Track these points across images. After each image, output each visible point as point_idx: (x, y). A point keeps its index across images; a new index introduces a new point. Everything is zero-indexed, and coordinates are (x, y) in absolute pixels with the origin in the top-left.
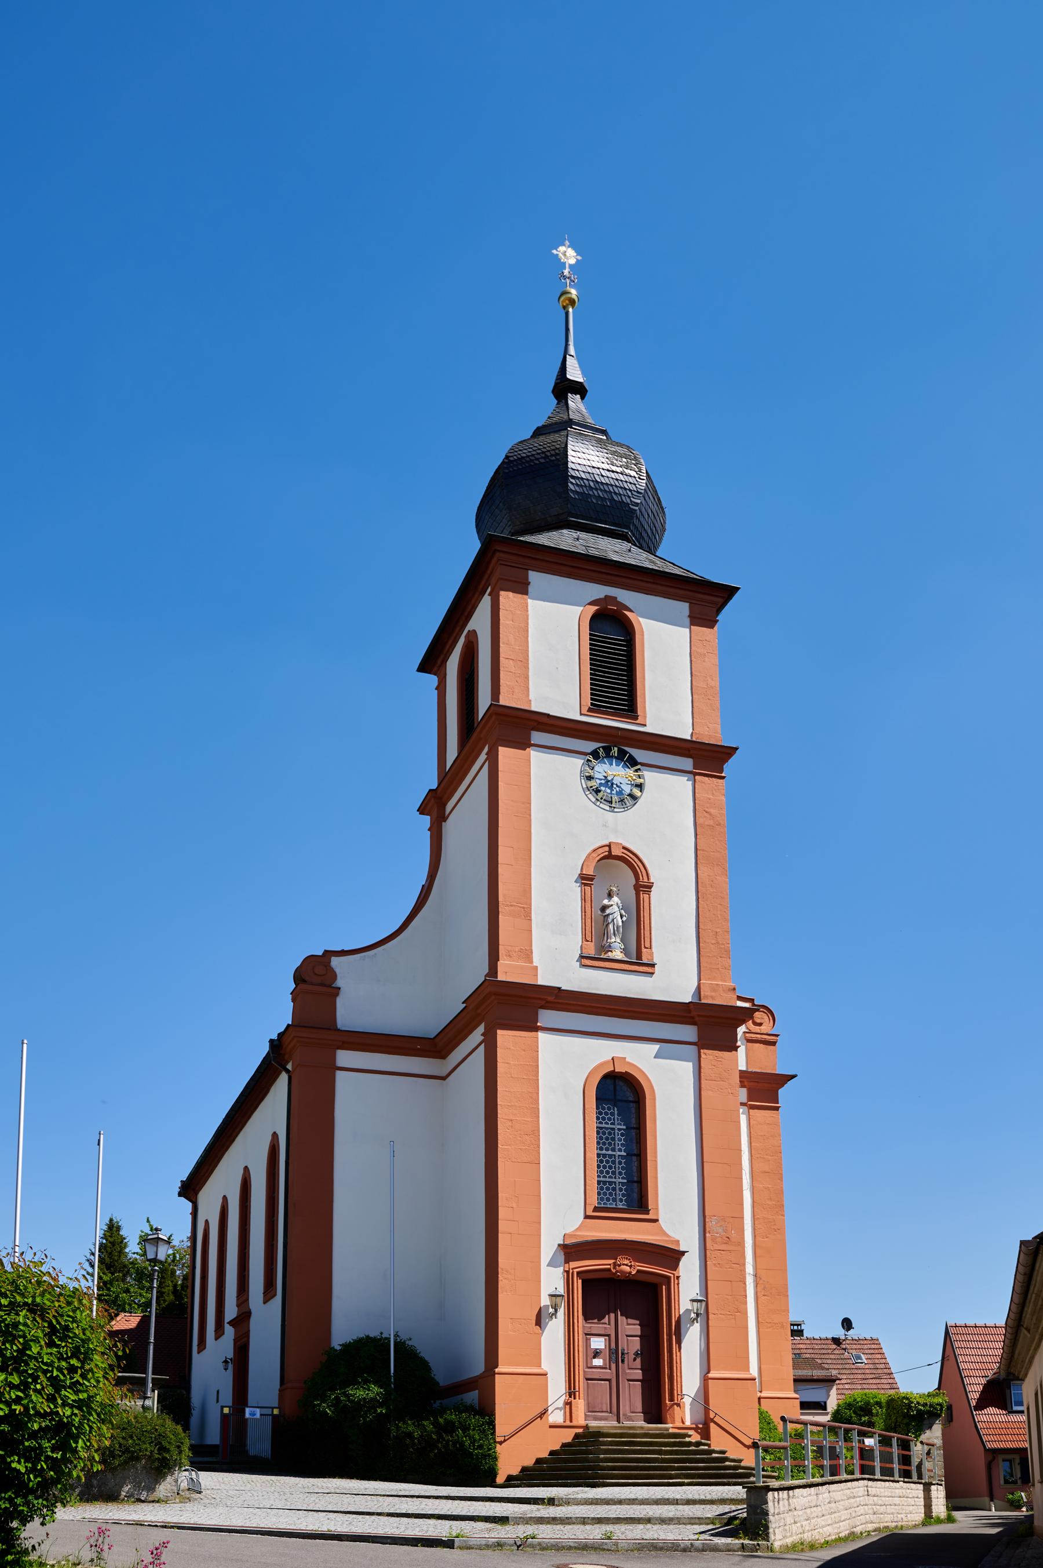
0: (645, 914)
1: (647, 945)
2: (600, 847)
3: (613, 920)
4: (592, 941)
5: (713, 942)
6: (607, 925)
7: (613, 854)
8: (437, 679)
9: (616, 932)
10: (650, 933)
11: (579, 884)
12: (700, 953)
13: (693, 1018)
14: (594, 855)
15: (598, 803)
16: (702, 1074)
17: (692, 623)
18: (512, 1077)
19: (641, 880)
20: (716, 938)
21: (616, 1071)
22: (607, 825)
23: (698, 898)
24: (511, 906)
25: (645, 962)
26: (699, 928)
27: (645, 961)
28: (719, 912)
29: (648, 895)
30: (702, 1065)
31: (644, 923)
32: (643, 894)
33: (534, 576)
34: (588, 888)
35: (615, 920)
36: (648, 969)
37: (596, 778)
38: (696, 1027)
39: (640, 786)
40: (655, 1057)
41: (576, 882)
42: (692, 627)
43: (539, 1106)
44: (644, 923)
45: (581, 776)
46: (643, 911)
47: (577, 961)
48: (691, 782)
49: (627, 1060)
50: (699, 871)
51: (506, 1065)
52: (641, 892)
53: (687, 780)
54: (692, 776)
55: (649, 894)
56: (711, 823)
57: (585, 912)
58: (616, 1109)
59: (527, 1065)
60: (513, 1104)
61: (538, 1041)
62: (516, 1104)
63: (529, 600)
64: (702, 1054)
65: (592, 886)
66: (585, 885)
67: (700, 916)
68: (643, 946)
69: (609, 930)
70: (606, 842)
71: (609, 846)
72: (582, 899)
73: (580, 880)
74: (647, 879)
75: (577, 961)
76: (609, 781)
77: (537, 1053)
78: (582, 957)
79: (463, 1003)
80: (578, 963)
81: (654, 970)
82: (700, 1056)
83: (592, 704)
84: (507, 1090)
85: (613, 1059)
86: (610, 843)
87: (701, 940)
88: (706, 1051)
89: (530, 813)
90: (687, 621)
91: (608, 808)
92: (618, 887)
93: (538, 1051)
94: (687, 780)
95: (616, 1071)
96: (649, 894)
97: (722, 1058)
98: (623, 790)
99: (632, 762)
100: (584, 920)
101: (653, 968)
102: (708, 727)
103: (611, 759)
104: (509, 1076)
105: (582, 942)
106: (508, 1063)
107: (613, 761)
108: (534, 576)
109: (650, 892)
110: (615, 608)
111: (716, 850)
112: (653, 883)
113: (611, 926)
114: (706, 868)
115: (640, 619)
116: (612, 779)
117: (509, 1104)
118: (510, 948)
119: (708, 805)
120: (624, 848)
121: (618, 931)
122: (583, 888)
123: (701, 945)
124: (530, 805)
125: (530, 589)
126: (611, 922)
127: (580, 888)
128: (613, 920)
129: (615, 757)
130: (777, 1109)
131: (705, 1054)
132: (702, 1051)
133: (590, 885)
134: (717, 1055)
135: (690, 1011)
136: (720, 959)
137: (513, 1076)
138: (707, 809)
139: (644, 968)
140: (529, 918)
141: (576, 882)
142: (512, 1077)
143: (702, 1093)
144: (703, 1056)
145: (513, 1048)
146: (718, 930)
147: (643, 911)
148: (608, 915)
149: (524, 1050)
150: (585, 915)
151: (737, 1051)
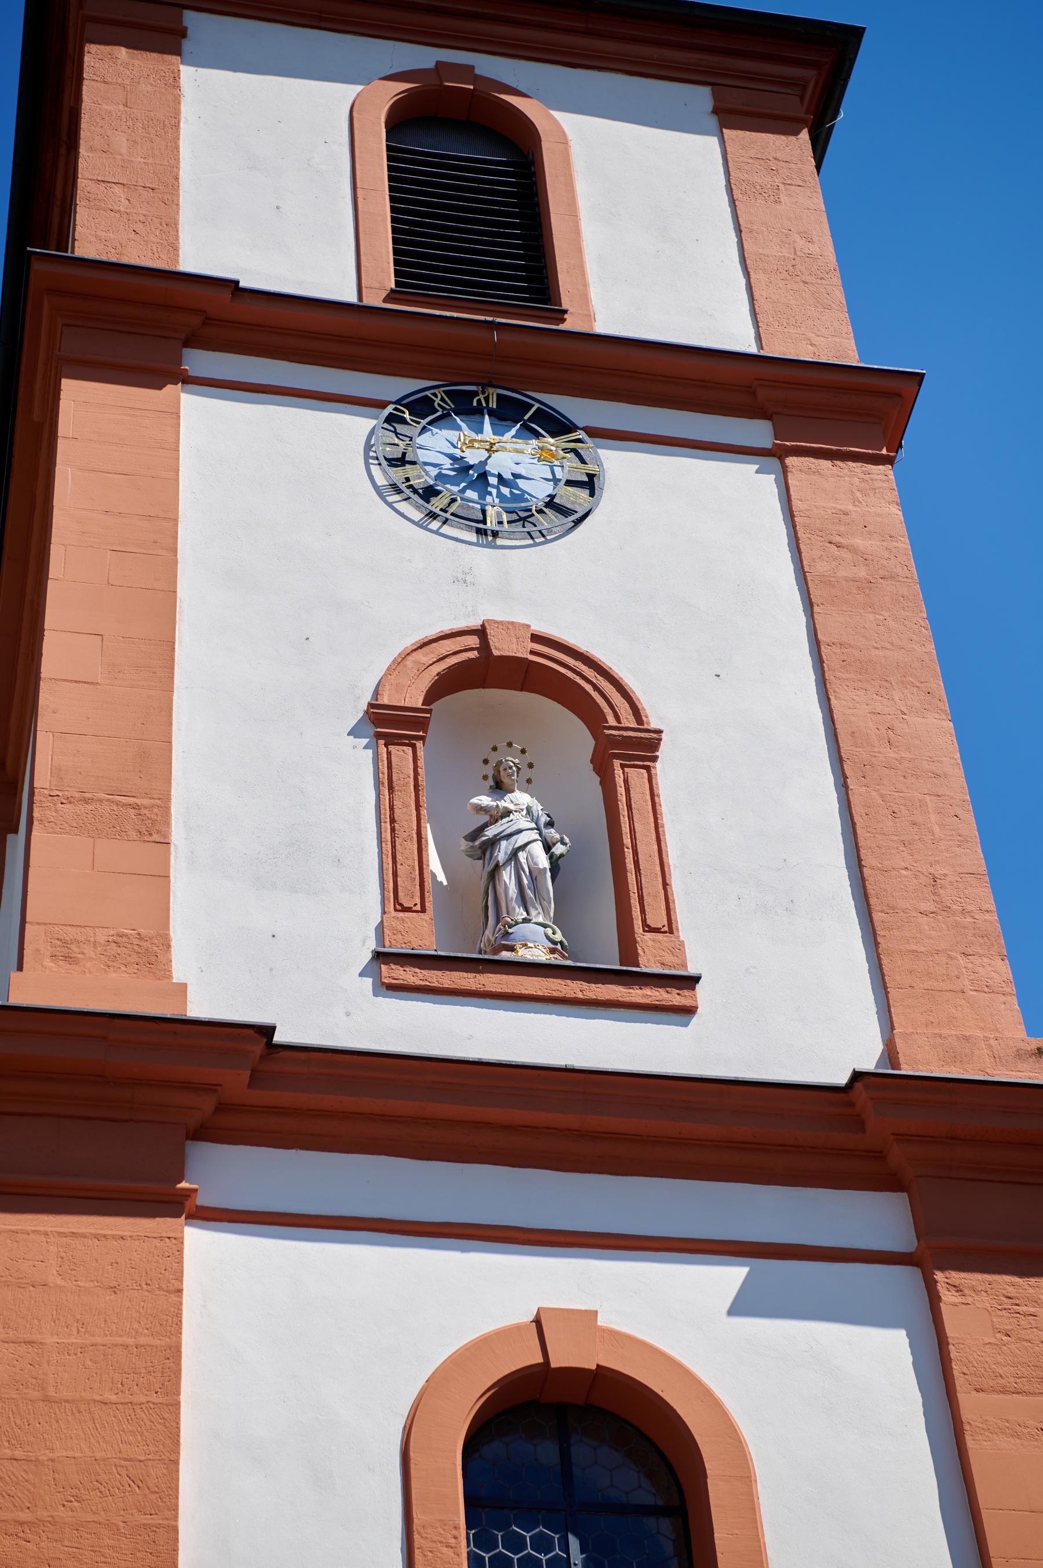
0: (638, 826)
1: (655, 917)
2: (421, 647)
3: (514, 855)
4: (423, 910)
5: (928, 906)
6: (494, 873)
7: (496, 653)
8: (438, 879)
9: (530, 894)
10: (665, 885)
11: (365, 741)
12: (877, 944)
13: (879, 1155)
14: (425, 657)
15: (435, 525)
16: (956, 1369)
17: (724, 124)
18: (46, 1399)
19: (612, 721)
20: (934, 894)
21: (553, 1365)
22: (469, 578)
23: (845, 777)
24: (86, 801)
25: (644, 970)
26: (861, 866)
27: (648, 964)
28: (933, 818)
29: (644, 771)
30: (951, 1330)
31: (635, 853)
32: (623, 766)
33: (191, 19)
34: (402, 755)
35: (522, 856)
36: (665, 996)
37: (426, 464)
38: (904, 1196)
39: (590, 484)
40: (731, 1312)
41: (354, 732)
42: (724, 130)
43: (176, 1517)
44: (635, 853)
45: (367, 457)
46: (631, 818)
47: (362, 974)
48: (773, 476)
49: (601, 1322)
50: (833, 701)
51: (23, 1349)
52: (617, 763)
53: (757, 472)
54: (774, 462)
55: (648, 769)
56: (862, 572)
57: (393, 820)
58: (574, 1543)
59: (126, 1347)
60: (43, 1514)
61: (181, 1251)
62: (62, 1513)
63: (182, 68)
64: (942, 1289)
65: (419, 744)
66: (390, 740)
67: (859, 831)
68: (638, 924)
69: (500, 890)
70: (475, 623)
71: (481, 632)
72: (378, 784)
73: (371, 730)
74: (632, 718)
75: (362, 974)
76: (471, 467)
77: (173, 1298)
78: (380, 957)
79: (513, 474)
80: (369, 981)
81: (694, 998)
82: (934, 1300)
83: (397, 284)
84: (18, 1453)
85: (538, 1322)
86: (483, 626)
87: (873, 901)
88: (956, 1277)
89: (175, 543)
90: (713, 121)
91: (473, 537)
92: (523, 751)
93: (180, 1291)
94: (757, 472)
95: (553, 1365)
96: (648, 769)
97: (1036, 1302)
98: (524, 492)
99: (559, 426)
100: (388, 847)
101: (686, 992)
102: (812, 344)
103: (477, 417)
104: (36, 1394)
105: (384, 912)
106: (30, 1343)
107: (482, 423)
108: (191, 19)
109: (655, 759)
110: (472, 87)
111: (892, 644)
112: (660, 732)
113: (507, 876)
114: (861, 693)
115: (556, 114)
116: (484, 463)
117: (24, 1516)
118: (72, 933)
119: (843, 529)
120: (536, 638)
121: (535, 891)
122: (383, 750)
123: (877, 916)
124: (176, 525)
125: (187, 45)
126: (508, 861)
127: (370, 752)
128: (514, 855)
129: (492, 413)
130: (689, 1011)
131: (958, 1289)
132: (939, 1276)
133: (410, 742)
134: (1011, 1291)
135: (859, 1123)
136: (962, 961)
137: (51, 1392)
138: (838, 539)
139: (648, 991)
140: (156, 837)
141: (354, 732)
142: (46, 1399)
143: (970, 1442)
144: (947, 1296)
145: (59, 1281)
146: (938, 871)
147: (631, 818)
148: (494, 842)
149: (114, 1290)
150: (393, 830)
151: (694, 989)
